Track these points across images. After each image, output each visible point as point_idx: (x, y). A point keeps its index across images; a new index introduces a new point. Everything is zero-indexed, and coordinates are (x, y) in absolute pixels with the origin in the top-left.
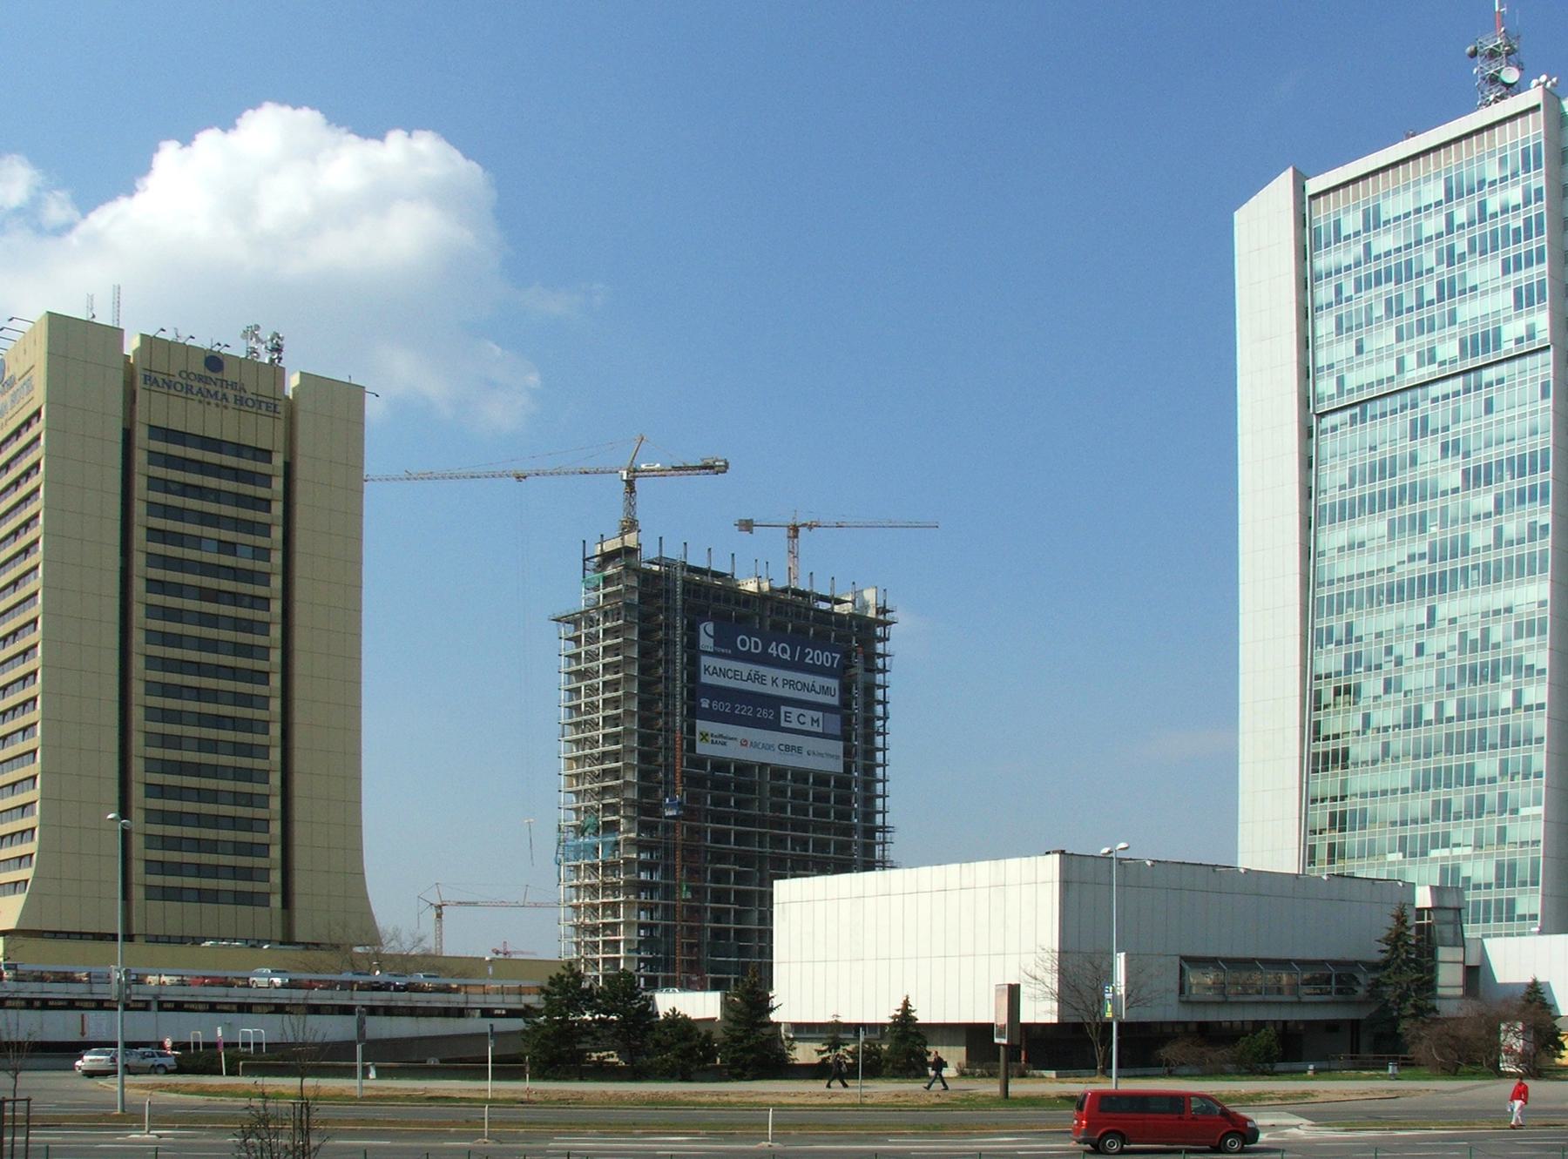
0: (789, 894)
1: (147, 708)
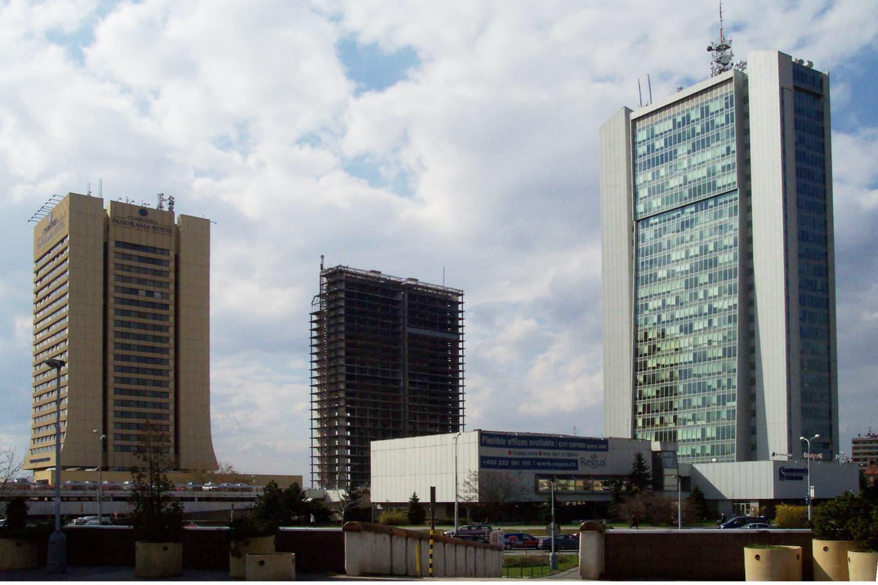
0: (375, 445)
1: (115, 320)
